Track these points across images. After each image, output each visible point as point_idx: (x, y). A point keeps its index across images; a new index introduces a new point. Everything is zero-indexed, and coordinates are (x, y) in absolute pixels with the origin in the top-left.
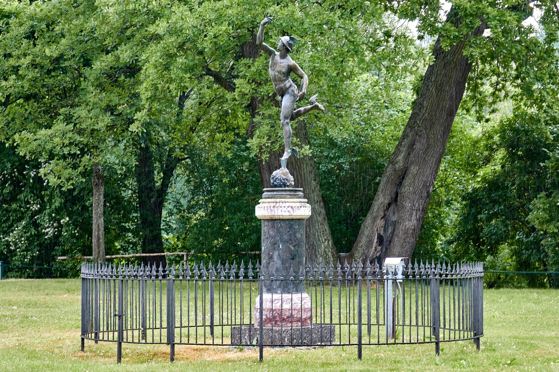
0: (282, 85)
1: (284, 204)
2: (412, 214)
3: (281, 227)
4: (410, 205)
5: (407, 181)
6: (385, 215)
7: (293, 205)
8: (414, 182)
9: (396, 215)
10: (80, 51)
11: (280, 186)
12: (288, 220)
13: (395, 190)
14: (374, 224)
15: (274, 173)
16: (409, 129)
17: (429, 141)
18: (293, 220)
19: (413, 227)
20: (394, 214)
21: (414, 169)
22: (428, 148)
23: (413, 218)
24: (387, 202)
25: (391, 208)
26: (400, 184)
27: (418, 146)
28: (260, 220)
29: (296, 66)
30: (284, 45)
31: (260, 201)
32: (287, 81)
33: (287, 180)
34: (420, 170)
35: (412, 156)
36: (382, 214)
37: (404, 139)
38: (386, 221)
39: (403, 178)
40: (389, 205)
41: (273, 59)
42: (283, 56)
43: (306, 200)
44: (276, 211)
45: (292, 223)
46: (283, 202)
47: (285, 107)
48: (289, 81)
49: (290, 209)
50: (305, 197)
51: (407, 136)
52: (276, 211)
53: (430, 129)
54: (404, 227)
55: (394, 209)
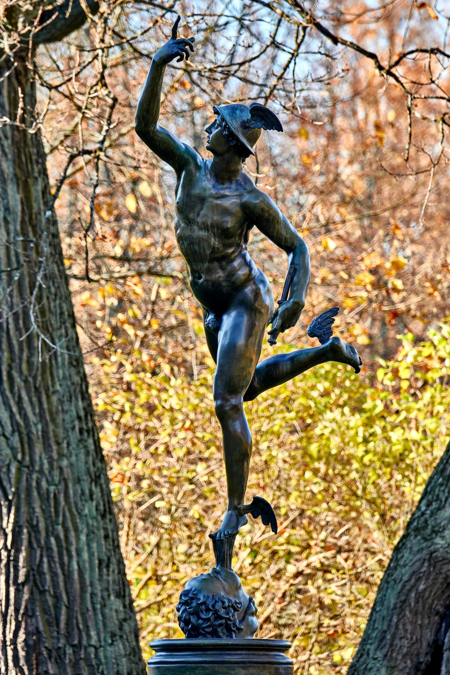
11: (215, 634)
13: (429, 636)
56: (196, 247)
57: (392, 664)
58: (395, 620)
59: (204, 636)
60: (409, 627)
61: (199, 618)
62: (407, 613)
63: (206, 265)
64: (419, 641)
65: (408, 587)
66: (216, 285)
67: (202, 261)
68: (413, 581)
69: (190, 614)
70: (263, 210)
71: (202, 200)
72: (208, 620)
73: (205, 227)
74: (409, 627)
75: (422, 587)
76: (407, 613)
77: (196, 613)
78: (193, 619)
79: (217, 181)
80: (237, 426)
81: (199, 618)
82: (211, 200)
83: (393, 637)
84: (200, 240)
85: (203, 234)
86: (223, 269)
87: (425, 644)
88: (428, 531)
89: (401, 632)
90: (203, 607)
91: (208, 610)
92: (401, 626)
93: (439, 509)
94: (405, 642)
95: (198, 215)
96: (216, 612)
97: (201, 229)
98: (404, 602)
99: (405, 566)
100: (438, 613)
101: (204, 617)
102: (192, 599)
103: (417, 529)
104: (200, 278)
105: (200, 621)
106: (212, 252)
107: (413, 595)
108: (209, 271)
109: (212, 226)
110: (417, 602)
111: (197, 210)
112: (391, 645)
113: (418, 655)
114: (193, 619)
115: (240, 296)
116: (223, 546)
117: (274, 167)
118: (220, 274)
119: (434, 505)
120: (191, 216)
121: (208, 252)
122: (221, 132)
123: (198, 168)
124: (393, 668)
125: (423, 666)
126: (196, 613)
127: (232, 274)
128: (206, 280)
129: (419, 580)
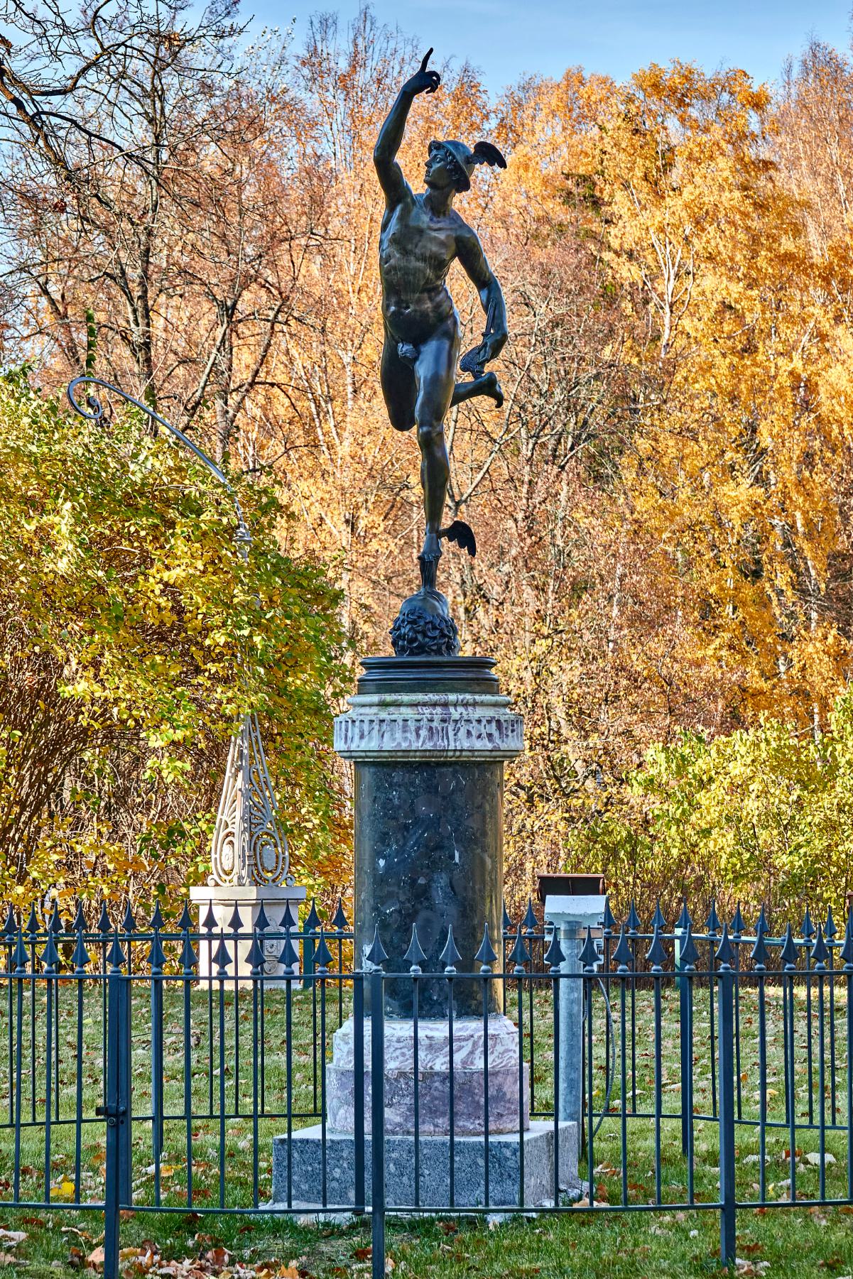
11: (439, 652)
56: (411, 278)
59: (429, 654)
61: (425, 636)
71: (421, 232)
72: (434, 638)
73: (423, 258)
79: (433, 214)
80: (439, 454)
84: (417, 270)
85: (420, 264)
86: (431, 299)
91: (434, 628)
96: (442, 630)
97: (418, 260)
106: (426, 283)
108: (419, 301)
109: (431, 257)
116: (428, 566)
117: (484, 204)
118: (428, 305)
120: (410, 247)
121: (422, 283)
122: (445, 166)
123: (414, 202)
128: (415, 311)
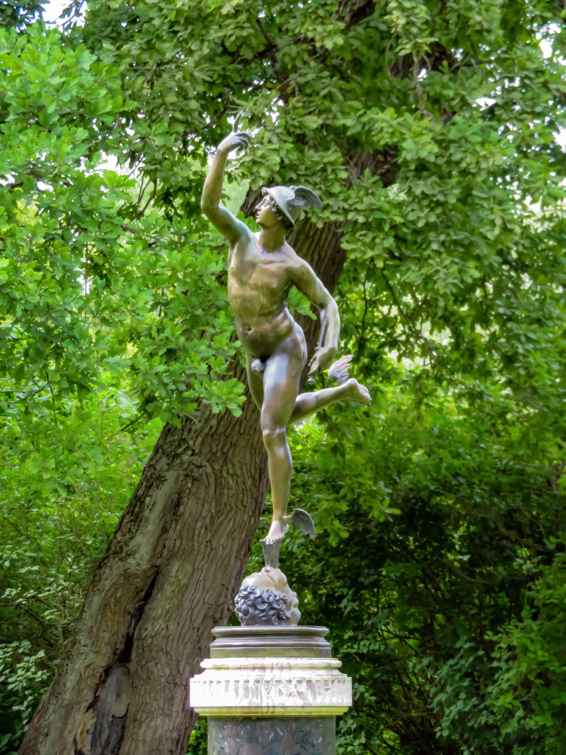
0: (267, 327)
1: (286, 675)
2: (172, 698)
3: (277, 739)
4: (167, 672)
5: (161, 604)
6: (96, 699)
7: (313, 675)
8: (179, 607)
9: (125, 699)
10: (179, 222)
11: (268, 622)
12: (297, 719)
13: (123, 630)
14: (65, 724)
15: (249, 581)
16: (165, 460)
17: (221, 494)
18: (309, 719)
19: (175, 735)
20: (118, 695)
21: (177, 572)
22: (219, 512)
23: (174, 709)
24: (102, 662)
25: (112, 679)
26: (139, 614)
27: (189, 507)
28: (205, 718)
29: (308, 272)
30: (279, 212)
31: (203, 664)
32: (281, 316)
33: (285, 602)
34: (197, 576)
35: (172, 535)
36: (90, 698)
37: (149, 487)
38: (100, 716)
39: (148, 596)
40: (108, 671)
41: (242, 252)
42: (271, 245)
43: (336, 662)
44: (264, 693)
45: (307, 728)
46: (282, 668)
47: (275, 389)
48: (286, 317)
49: (303, 688)
50: (335, 653)
51: (161, 479)
52: (264, 693)
53: (225, 461)
54: (150, 734)
55: (118, 682)
56: (248, 305)
57: (97, 649)
58: (99, 618)
60: (110, 623)
62: (109, 613)
63: (255, 319)
64: (117, 633)
65: (109, 595)
66: (264, 336)
67: (252, 316)
68: (112, 590)
69: (249, 606)
70: (303, 273)
71: (253, 265)
72: (263, 611)
74: (110, 623)
75: (119, 595)
76: (109, 613)
77: (254, 606)
78: (251, 610)
81: (256, 609)
82: (261, 265)
83: (98, 630)
87: (120, 636)
88: (123, 555)
89: (104, 627)
90: (260, 600)
91: (263, 602)
92: (104, 623)
93: (131, 539)
94: (107, 635)
95: (250, 277)
97: (252, 289)
98: (106, 605)
99: (107, 579)
100: (130, 613)
101: (260, 608)
102: (250, 593)
103: (115, 553)
104: (250, 329)
105: (257, 612)
107: (113, 600)
109: (262, 286)
110: (116, 605)
111: (249, 273)
112: (97, 636)
113: (116, 643)
114: (251, 610)
115: (283, 345)
119: (128, 536)
120: (244, 278)
121: (258, 308)
124: (98, 652)
125: (119, 652)
126: (254, 606)
127: (276, 327)
128: (255, 332)
129: (117, 589)
